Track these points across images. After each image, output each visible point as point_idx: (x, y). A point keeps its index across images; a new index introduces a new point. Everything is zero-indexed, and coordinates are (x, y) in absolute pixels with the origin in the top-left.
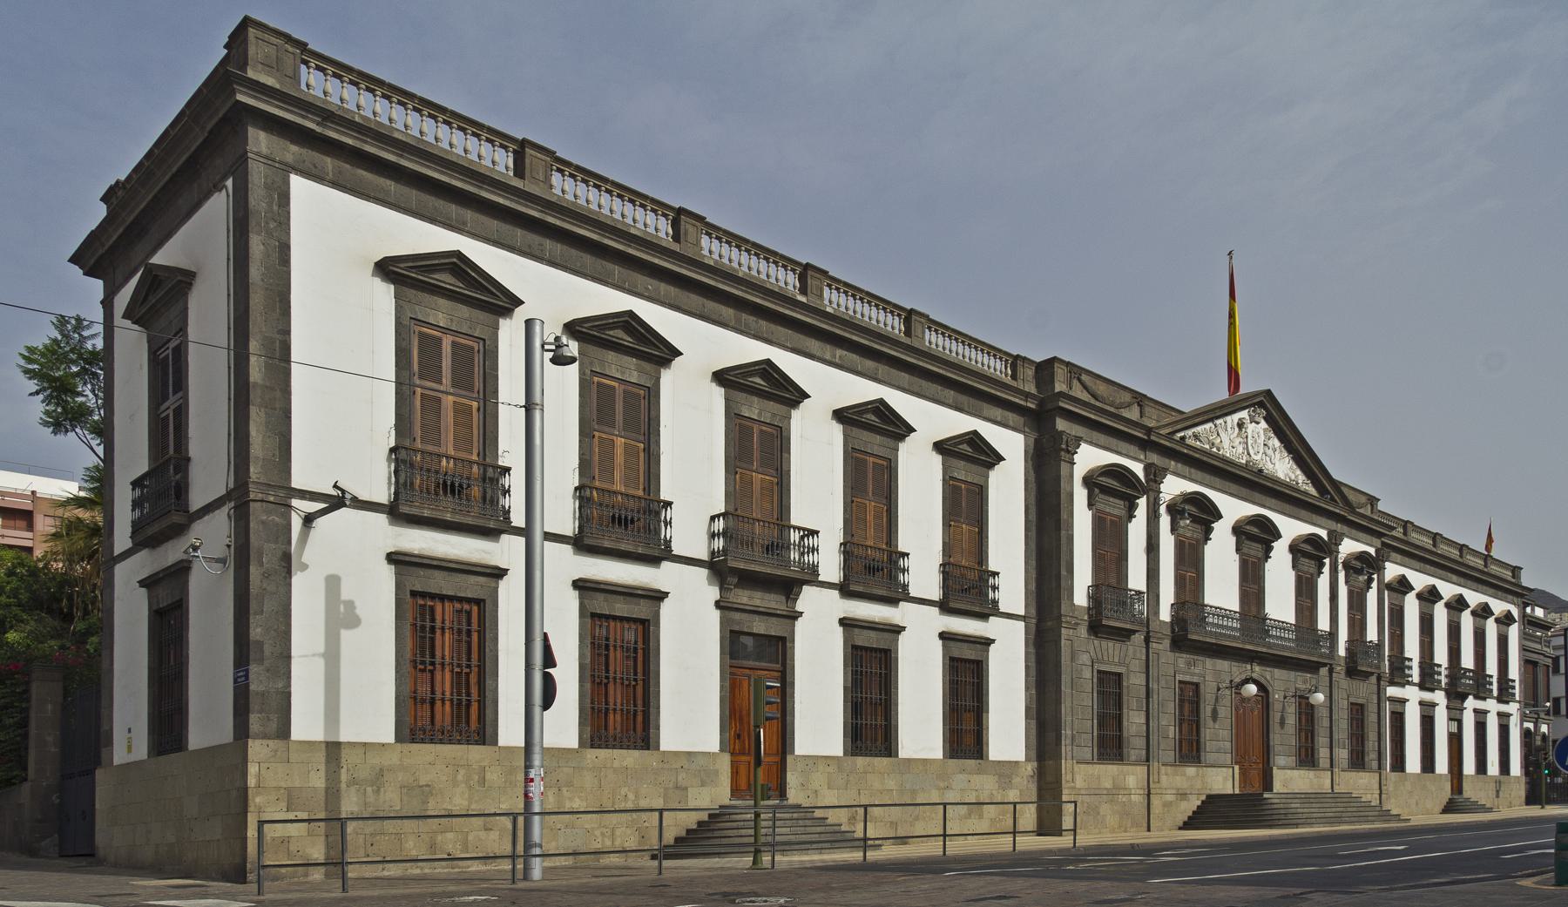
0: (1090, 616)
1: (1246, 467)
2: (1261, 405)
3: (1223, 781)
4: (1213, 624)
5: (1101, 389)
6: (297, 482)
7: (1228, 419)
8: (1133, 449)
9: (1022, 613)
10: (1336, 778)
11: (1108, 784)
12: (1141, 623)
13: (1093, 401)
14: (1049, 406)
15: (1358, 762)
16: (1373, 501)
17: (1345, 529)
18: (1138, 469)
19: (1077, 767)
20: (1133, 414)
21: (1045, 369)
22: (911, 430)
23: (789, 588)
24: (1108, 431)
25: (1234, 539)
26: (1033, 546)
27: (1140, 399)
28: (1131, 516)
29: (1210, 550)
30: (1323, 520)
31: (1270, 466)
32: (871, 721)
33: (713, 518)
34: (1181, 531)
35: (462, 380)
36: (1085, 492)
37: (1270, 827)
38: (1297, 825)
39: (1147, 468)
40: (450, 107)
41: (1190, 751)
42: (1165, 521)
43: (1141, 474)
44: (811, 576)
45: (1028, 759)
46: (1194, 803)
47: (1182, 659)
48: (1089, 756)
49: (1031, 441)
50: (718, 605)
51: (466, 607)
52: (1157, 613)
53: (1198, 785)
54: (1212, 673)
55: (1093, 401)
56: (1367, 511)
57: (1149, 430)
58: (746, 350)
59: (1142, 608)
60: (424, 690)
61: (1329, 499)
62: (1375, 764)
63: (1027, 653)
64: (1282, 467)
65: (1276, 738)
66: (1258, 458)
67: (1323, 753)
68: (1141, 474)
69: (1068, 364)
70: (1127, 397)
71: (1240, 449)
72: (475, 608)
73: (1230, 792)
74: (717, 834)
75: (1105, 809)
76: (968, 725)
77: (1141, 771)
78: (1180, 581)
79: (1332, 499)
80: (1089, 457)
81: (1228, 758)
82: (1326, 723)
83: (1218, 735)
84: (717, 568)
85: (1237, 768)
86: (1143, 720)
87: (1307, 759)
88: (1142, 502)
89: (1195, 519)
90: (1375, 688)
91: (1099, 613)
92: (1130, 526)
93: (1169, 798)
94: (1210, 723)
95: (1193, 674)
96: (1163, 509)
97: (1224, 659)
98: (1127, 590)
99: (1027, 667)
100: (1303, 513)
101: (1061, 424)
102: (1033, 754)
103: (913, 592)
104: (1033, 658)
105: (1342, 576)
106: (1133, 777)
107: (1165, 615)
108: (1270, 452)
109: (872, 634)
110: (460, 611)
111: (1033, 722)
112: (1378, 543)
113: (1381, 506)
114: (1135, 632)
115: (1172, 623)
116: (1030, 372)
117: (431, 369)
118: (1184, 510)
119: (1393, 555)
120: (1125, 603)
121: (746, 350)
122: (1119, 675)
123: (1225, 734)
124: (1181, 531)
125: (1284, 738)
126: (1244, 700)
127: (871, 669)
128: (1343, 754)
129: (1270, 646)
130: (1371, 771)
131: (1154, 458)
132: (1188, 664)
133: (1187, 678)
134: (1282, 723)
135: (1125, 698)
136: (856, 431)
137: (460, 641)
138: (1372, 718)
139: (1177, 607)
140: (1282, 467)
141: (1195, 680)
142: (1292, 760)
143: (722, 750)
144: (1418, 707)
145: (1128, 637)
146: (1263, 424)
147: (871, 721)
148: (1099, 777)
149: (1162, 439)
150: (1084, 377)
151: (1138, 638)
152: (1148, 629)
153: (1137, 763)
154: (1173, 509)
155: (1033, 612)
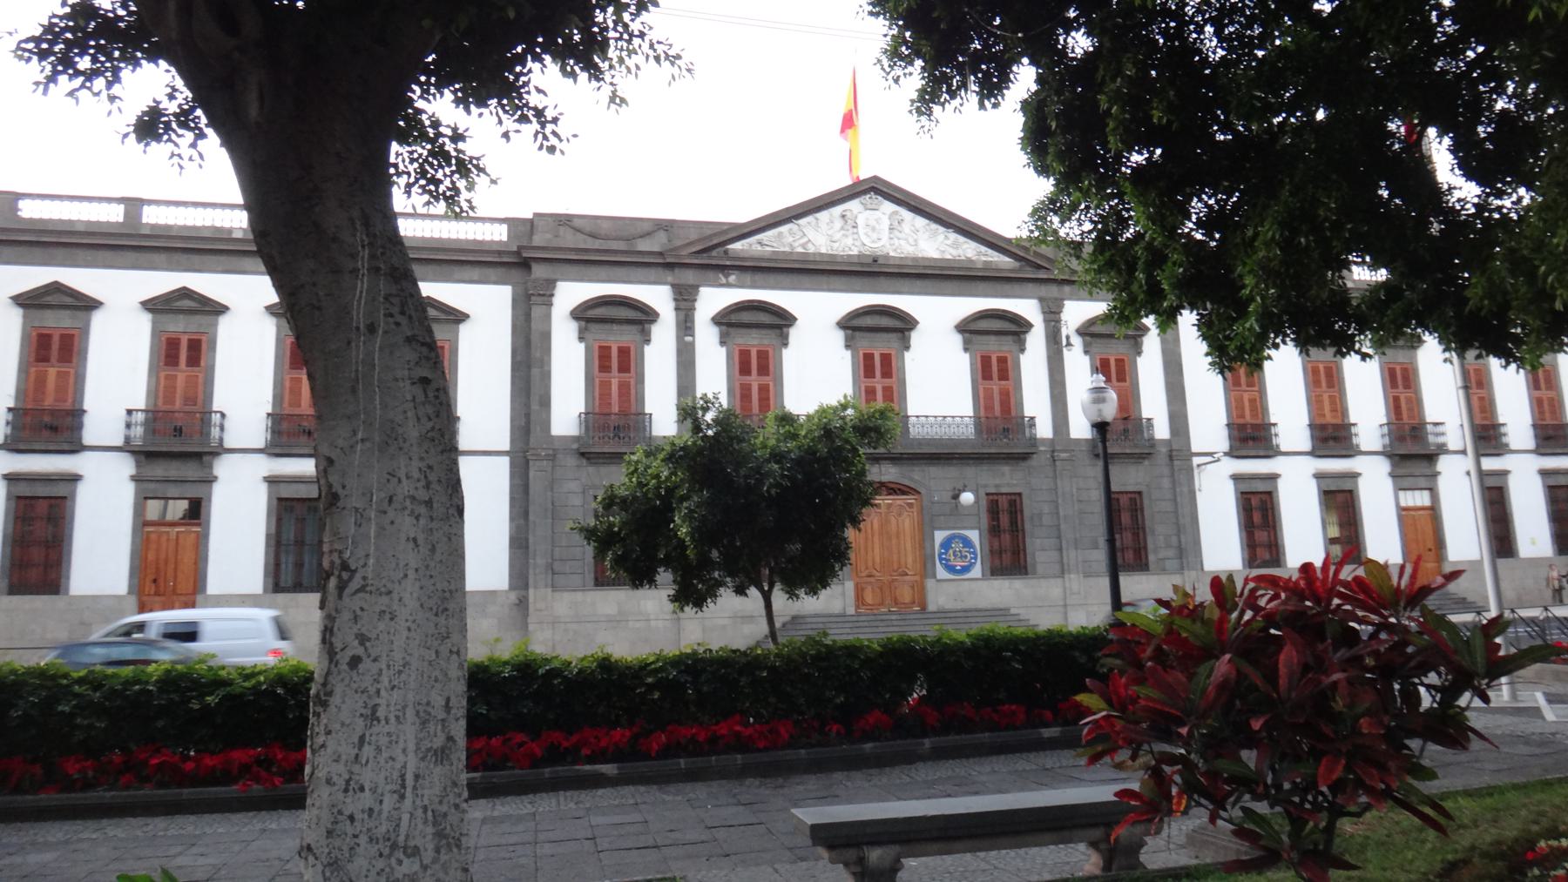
6: (1194, 449)
22: (795, 319)
23: (1431, 458)
32: (1501, 538)
33: (223, 415)
35: (1331, 385)
44: (1442, 449)
50: (134, 478)
58: (163, 282)
60: (996, 544)
64: (969, 251)
76: (1261, 536)
84: (1387, 453)
103: (1513, 447)
109: (302, 486)
121: (163, 282)
127: (1495, 501)
131: (1045, 290)
136: (164, 318)
143: (130, 593)
147: (1501, 538)
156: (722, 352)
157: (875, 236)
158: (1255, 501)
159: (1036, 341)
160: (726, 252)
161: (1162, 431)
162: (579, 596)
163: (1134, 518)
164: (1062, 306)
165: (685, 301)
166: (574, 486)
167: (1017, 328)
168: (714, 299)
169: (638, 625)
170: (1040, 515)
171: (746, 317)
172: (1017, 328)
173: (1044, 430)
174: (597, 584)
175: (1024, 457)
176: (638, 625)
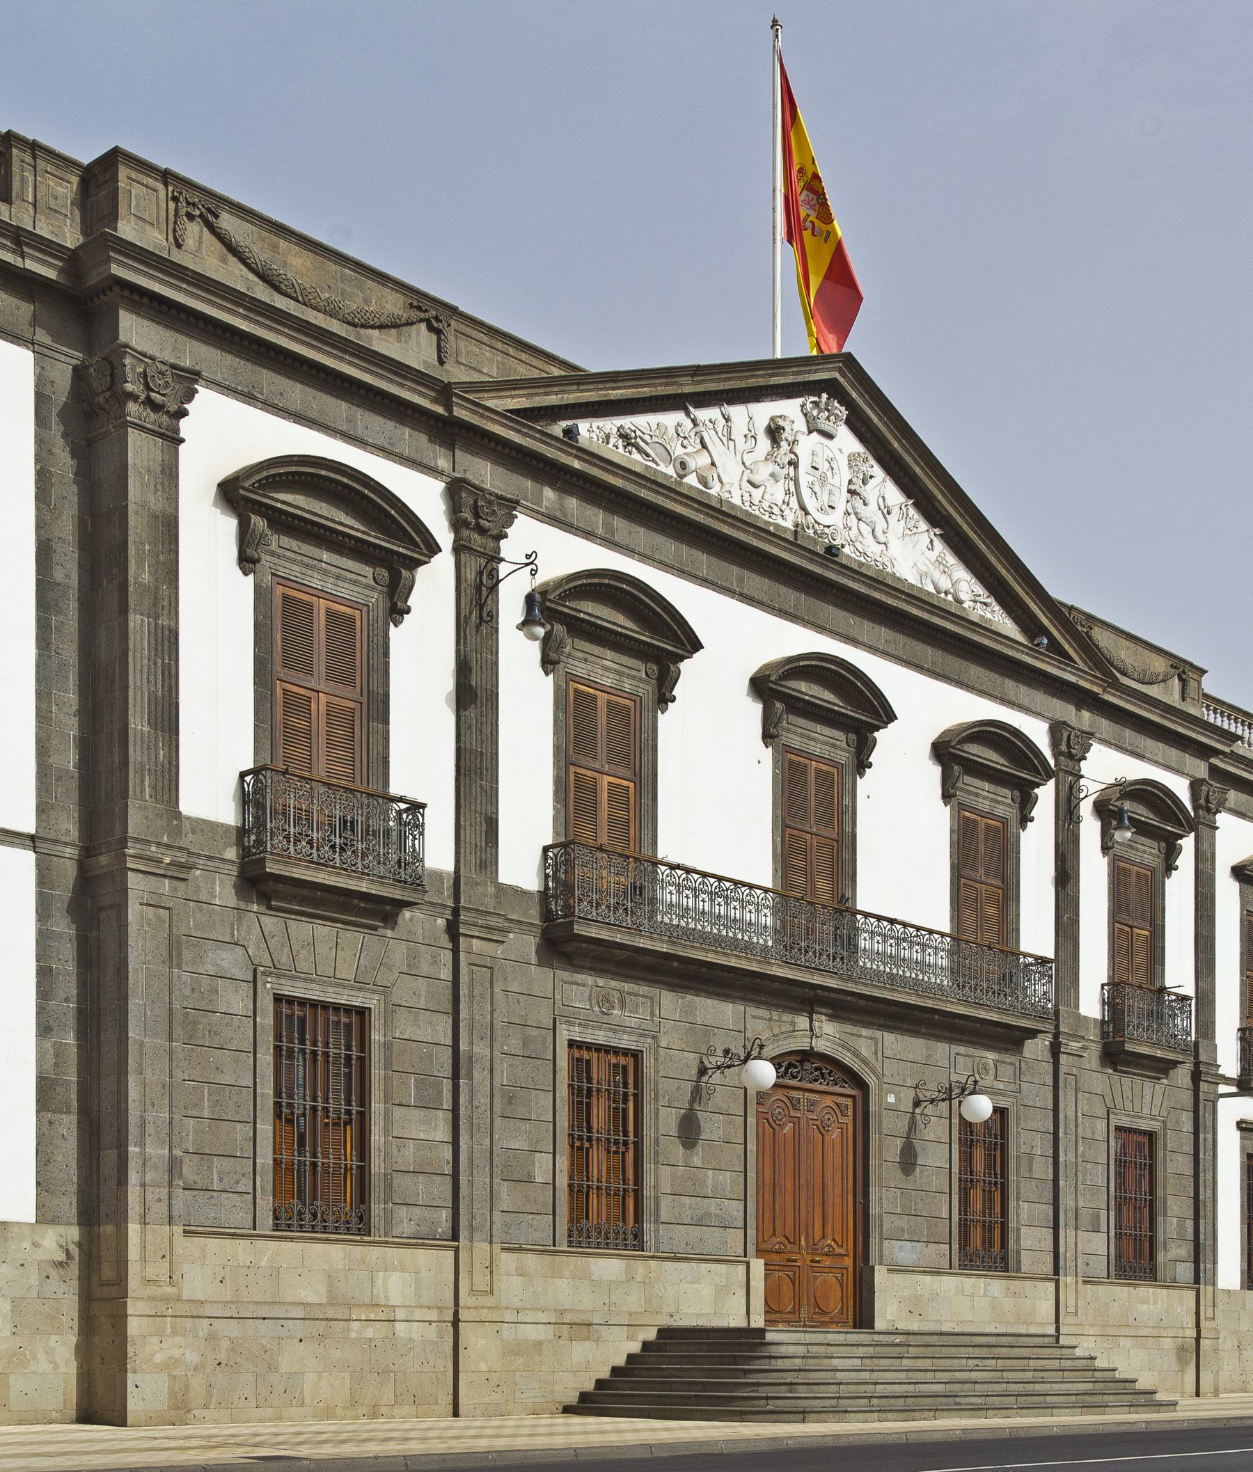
0: (1104, 1035)
1: (795, 541)
2: (833, 389)
3: (715, 1293)
4: (872, 955)
5: (297, 265)
7: (738, 412)
8: (408, 438)
9: (28, 824)
10: (1068, 1298)
11: (312, 1292)
12: (1042, 1017)
13: (262, 292)
14: (94, 279)
15: (1136, 1260)
16: (1185, 671)
17: (1105, 725)
18: (1037, 731)
19: (186, 1246)
20: (416, 349)
21: (99, 181)
24: (273, 360)
25: (937, 771)
26: (69, 652)
27: (434, 314)
28: (1170, 868)
29: (675, 730)
30: (1039, 698)
31: (873, 549)
34: (1117, 849)
36: (1097, 825)
37: (741, 1416)
38: (802, 1415)
39: (1056, 729)
40: (1228, 701)
41: (606, 1209)
42: (1090, 829)
43: (1184, 795)
45: (45, 1216)
46: (619, 1347)
47: (581, 989)
48: (241, 1217)
49: (62, 376)
51: (623, 1061)
52: (489, 863)
53: (633, 1301)
54: (665, 1027)
55: (262, 292)
56: (1170, 693)
57: (445, 392)
59: (1186, 1025)
61: (1049, 648)
62: (1185, 1271)
63: (44, 939)
64: (912, 555)
65: (886, 1197)
66: (835, 519)
67: (1031, 1241)
68: (1184, 795)
69: (166, 176)
70: (1159, 665)
71: (777, 492)
72: (631, 1060)
73: (735, 1320)
74: (779, 1364)
75: (295, 1357)
77: (434, 1264)
78: (573, 795)
79: (1055, 647)
80: (226, 432)
81: (734, 1242)
82: (1043, 1169)
83: (701, 1182)
85: (758, 1266)
86: (442, 1133)
87: (984, 1244)
88: (1046, 794)
89: (1141, 828)
90: (1187, 1098)
91: (1119, 1030)
92: (1169, 883)
93: (533, 1333)
94: (677, 1152)
95: (621, 1029)
96: (1086, 808)
97: (726, 997)
98: (1017, 954)
99: (44, 974)
100: (976, 672)
101: (135, 330)
102: (68, 1204)
104: (66, 954)
105: (1090, 829)
106: (399, 1278)
107: (1090, 1004)
108: (871, 512)
110: (616, 1066)
111: (68, 1125)
112: (1200, 769)
113: (1209, 685)
114: (1033, 1033)
115: (544, 895)
116: (65, 190)
117: (298, 659)
118: (1121, 811)
119: (1233, 796)
120: (1160, 1016)
122: (362, 1013)
123: (727, 1180)
124: (1117, 849)
125: (914, 1201)
126: (966, 1126)
128: (1095, 1246)
129: (658, 931)
130: (1173, 1284)
132: (605, 1002)
133: (600, 1037)
134: (908, 1161)
135: (377, 1074)
137: (580, 1103)
138: (1174, 1164)
139: (1115, 989)
140: (912, 555)
141: (626, 1042)
142: (938, 1253)
144: (1237, 1134)
145: (1165, 1072)
146: (847, 442)
148: (275, 1273)
149: (524, 432)
150: (227, 222)
151: (1182, 1075)
152: (467, 904)
153: (419, 1241)
154: (543, 607)
155: (68, 826)
156: (546, 685)
157: (824, 497)
158: (599, 1072)
159: (435, 586)
160: (571, 433)
161: (438, 850)
162: (241, 1250)
163: (618, 1118)
164: (1087, 748)
165: (479, 522)
166: (230, 961)
167: (392, 543)
168: (545, 549)
169: (369, 1332)
170: (1031, 1157)
171: (805, 689)
172: (392, 543)
173: (438, 850)
174: (1118, 1277)
175: (383, 912)
176: (369, 1332)
